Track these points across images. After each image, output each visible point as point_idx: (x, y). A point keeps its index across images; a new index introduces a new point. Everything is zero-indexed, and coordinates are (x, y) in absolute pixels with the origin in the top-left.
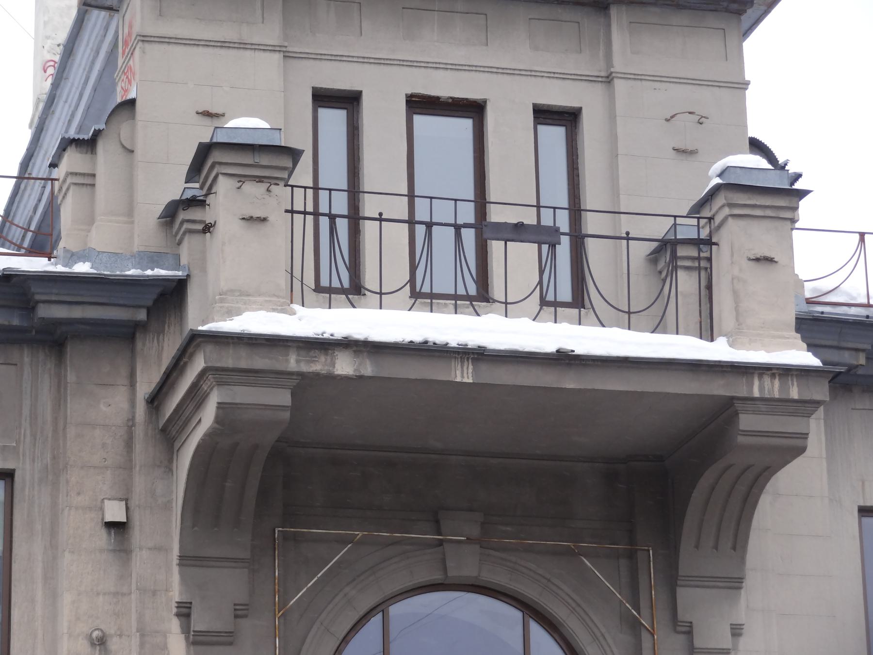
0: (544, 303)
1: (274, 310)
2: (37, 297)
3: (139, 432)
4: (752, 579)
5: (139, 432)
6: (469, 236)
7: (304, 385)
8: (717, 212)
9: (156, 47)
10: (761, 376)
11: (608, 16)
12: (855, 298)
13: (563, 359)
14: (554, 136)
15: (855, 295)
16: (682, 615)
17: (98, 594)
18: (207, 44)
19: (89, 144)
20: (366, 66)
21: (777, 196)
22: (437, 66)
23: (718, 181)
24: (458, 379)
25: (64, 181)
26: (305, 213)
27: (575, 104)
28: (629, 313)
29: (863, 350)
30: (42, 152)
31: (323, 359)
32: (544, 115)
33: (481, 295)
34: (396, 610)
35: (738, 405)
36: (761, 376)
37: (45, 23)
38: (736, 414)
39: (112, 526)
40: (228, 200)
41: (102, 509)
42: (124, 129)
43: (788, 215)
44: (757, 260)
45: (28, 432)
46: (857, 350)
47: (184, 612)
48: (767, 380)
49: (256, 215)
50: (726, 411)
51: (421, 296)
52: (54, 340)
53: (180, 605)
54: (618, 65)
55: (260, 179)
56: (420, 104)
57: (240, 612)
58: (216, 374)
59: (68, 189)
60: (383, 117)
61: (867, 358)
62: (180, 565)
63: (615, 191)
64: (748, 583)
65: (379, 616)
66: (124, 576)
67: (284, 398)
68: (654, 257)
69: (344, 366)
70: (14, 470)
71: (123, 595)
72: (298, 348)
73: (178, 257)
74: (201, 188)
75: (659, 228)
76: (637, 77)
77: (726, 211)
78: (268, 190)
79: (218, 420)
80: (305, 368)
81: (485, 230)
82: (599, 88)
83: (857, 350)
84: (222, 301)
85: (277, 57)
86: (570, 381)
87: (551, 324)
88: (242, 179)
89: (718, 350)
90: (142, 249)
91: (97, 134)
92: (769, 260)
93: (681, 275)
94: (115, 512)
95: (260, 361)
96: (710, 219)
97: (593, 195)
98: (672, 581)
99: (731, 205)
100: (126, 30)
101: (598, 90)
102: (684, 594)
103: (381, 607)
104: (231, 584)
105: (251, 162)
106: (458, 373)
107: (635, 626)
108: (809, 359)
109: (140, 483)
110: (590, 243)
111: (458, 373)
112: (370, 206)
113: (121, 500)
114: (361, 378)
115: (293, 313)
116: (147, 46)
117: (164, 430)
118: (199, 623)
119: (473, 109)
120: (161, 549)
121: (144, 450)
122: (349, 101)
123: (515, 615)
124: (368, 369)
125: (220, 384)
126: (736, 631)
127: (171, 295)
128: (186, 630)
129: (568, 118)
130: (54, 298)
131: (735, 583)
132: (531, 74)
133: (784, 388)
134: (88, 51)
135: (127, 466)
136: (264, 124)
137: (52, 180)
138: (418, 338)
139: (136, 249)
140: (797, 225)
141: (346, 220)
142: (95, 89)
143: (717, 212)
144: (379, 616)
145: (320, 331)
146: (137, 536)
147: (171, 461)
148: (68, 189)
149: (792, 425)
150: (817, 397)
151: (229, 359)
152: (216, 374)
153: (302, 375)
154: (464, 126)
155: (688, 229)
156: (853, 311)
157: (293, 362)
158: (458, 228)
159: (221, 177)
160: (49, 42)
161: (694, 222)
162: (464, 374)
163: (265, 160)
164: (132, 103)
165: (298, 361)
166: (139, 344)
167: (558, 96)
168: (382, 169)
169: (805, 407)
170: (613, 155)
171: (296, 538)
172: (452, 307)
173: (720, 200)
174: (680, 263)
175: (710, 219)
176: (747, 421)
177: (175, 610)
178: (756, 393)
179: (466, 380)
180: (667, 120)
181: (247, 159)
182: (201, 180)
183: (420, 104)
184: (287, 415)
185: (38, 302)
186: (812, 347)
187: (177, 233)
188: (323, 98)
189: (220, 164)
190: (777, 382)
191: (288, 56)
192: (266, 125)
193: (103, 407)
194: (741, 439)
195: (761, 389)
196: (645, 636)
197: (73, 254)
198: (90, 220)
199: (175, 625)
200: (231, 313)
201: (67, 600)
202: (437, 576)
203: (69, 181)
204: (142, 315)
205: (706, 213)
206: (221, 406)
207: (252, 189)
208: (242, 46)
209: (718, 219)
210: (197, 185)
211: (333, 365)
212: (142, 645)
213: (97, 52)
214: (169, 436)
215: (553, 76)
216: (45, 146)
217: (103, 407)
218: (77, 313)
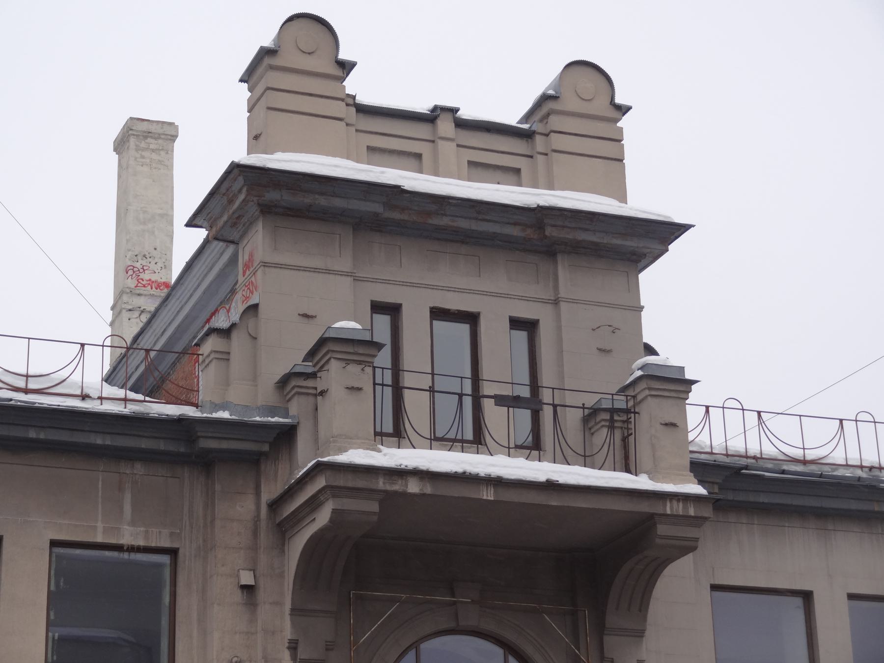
0: (376, 434)
1: (367, 449)
2: (199, 434)
4: (650, 631)
5: (263, 524)
7: (387, 498)
8: (639, 393)
9: (273, 270)
10: (671, 500)
11: (555, 262)
12: (702, 448)
13: (551, 486)
14: (521, 336)
15: (703, 445)
16: (607, 654)
17: (236, 633)
18: (306, 269)
19: (226, 333)
20: (405, 287)
21: (677, 385)
22: (449, 289)
23: (639, 373)
24: (485, 498)
25: (208, 356)
26: (383, 385)
27: (536, 318)
28: (585, 456)
29: (717, 483)
30: (151, 330)
31: (400, 482)
32: (516, 323)
33: (478, 440)
34: (425, 646)
36: (671, 500)
37: (128, 241)
38: (655, 524)
39: (246, 588)
40: (336, 375)
41: (238, 576)
42: (251, 323)
43: (682, 396)
44: (666, 424)
45: (188, 523)
46: (713, 483)
47: (293, 646)
48: (675, 503)
49: (356, 386)
50: (648, 522)
51: (437, 440)
52: (206, 463)
53: (291, 641)
54: (562, 294)
55: (359, 362)
56: (439, 314)
57: (329, 648)
58: (332, 490)
59: (211, 361)
60: (415, 322)
61: (720, 489)
62: (290, 615)
63: (561, 376)
64: (647, 633)
65: (414, 651)
67: (373, 507)
68: (586, 420)
69: (413, 487)
70: (178, 549)
71: (252, 634)
72: (385, 475)
73: (287, 410)
74: (314, 366)
75: (590, 401)
77: (647, 392)
78: (363, 370)
79: (331, 520)
80: (388, 488)
83: (713, 483)
84: (334, 442)
85: (350, 279)
86: (554, 501)
87: (537, 463)
88: (348, 362)
89: (642, 482)
90: (264, 403)
91: (233, 325)
92: (674, 425)
93: (616, 431)
94: (247, 578)
96: (634, 397)
97: (547, 378)
98: (601, 629)
99: (650, 389)
100: (246, 257)
101: (549, 308)
102: (608, 640)
103: (415, 645)
105: (352, 351)
106: (485, 493)
108: (697, 489)
109: (263, 559)
110: (407, 394)
111: (485, 493)
112: (408, 380)
113: (250, 570)
114: (424, 495)
115: (379, 451)
116: (266, 269)
117: (279, 525)
118: (302, 654)
119: (471, 319)
121: (264, 538)
122: (393, 310)
123: (499, 651)
124: (428, 490)
125: (334, 496)
127: (286, 436)
129: (528, 326)
130: (210, 435)
131: (640, 634)
132: (507, 296)
133: (685, 508)
134: (204, 267)
135: (254, 548)
136: (358, 326)
137: (199, 355)
138: (460, 469)
139: (259, 404)
140: (687, 402)
141: (390, 388)
142: (204, 293)
143: (639, 393)
144: (414, 651)
145: (398, 464)
146: (262, 595)
147: (283, 545)
148: (211, 361)
149: (690, 532)
150: (706, 515)
151: (341, 481)
152: (332, 490)
153: (386, 492)
154: (464, 329)
155: (620, 403)
156: (703, 456)
157: (381, 484)
159: (332, 360)
160: (130, 253)
161: (623, 398)
162: (488, 494)
164: (255, 307)
165: (384, 483)
166: (263, 467)
167: (525, 312)
168: (414, 356)
169: (698, 521)
170: (560, 352)
172: (460, 448)
173: (643, 385)
174: (616, 424)
175: (634, 397)
176: (662, 529)
177: (287, 645)
178: (669, 512)
179: (489, 498)
180: (593, 330)
182: (315, 361)
183: (439, 314)
184: (375, 518)
185: (199, 437)
186: (701, 482)
187: (288, 394)
188: (378, 307)
189: (333, 351)
190: (681, 505)
191: (356, 280)
192: (360, 327)
193: (238, 508)
194: (658, 541)
195: (672, 508)
197: (216, 405)
198: (226, 383)
200: (342, 450)
202: (452, 625)
203: (213, 356)
204: (266, 448)
205: (631, 392)
206: (334, 511)
207: (353, 369)
208: (328, 271)
209: (639, 398)
210: (310, 364)
211: (407, 486)
213: (211, 269)
214: (284, 529)
216: (154, 327)
217: (238, 508)
218: (225, 445)
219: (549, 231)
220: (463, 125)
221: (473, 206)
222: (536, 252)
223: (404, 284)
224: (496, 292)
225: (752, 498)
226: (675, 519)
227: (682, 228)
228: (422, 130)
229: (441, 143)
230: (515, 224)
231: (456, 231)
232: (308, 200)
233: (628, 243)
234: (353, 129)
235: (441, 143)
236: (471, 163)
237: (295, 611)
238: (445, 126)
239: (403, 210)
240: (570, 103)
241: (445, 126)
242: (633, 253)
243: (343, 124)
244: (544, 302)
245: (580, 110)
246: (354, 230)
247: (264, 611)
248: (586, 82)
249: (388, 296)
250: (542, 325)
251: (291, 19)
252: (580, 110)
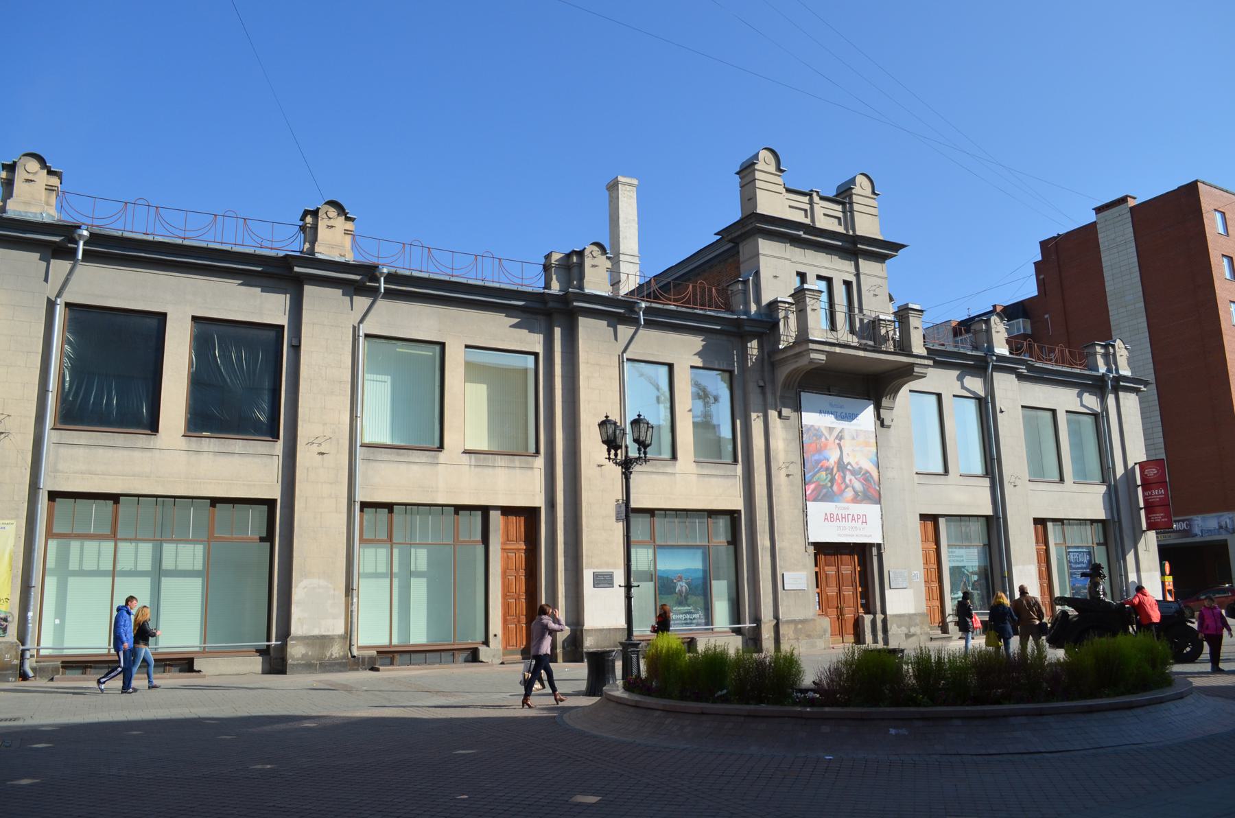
32: (799, 274)
94: (761, 384)
176: (916, 369)
227: (903, 246)
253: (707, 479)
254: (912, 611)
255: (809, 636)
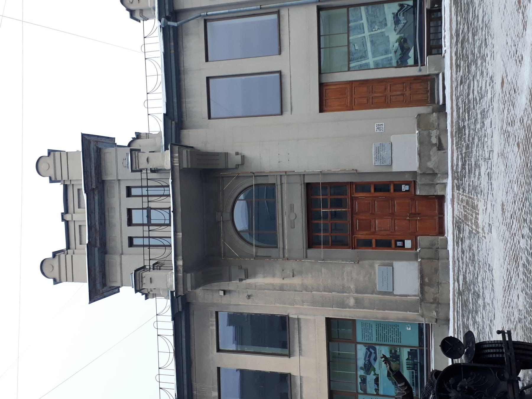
3: (205, 288)
6: (151, 228)
7: (185, 271)
22: (121, 220)
27: (125, 188)
35: (181, 168)
44: (148, 162)
48: (175, 162)
53: (240, 281)
57: (240, 268)
66: (235, 291)
67: (189, 275)
76: (117, 174)
80: (182, 272)
81: (149, 224)
82: (121, 182)
86: (179, 210)
94: (222, 293)
95: (181, 282)
98: (227, 169)
104: (234, 270)
107: (238, 177)
120: (228, 284)
123: (238, 202)
124: (181, 257)
126: (237, 154)
128: (245, 279)
131: (226, 154)
132: (120, 198)
133: (176, 157)
135: (212, 291)
157: (180, 275)
158: (149, 231)
162: (180, 235)
163: (138, 278)
167: (124, 192)
171: (224, 253)
176: (185, 166)
178: (178, 164)
181: (138, 282)
183: (130, 223)
191: (122, 254)
196: (240, 175)
199: (244, 281)
201: (240, 303)
202: (230, 222)
208: (121, 264)
212: (249, 289)
215: (120, 193)
219: (94, 187)
220: (67, 211)
221: (90, 215)
222: (103, 187)
223: (121, 236)
224: (119, 203)
225: (175, 105)
226: (180, 162)
228: (71, 225)
229: (74, 220)
230: (94, 198)
231: (100, 218)
232: (98, 274)
233: (93, 156)
234: (75, 251)
235: (74, 220)
236: (79, 207)
237: (230, 280)
238: (68, 217)
239: (96, 239)
240: (51, 172)
241: (68, 217)
242: (97, 151)
243: (73, 255)
244: (119, 184)
245: (50, 164)
246: (106, 254)
247: (230, 288)
248: (42, 166)
249: (126, 242)
250: (125, 196)
251: (43, 273)
252: (50, 164)
253: (303, 347)
254: (414, 139)
255: (436, 270)
